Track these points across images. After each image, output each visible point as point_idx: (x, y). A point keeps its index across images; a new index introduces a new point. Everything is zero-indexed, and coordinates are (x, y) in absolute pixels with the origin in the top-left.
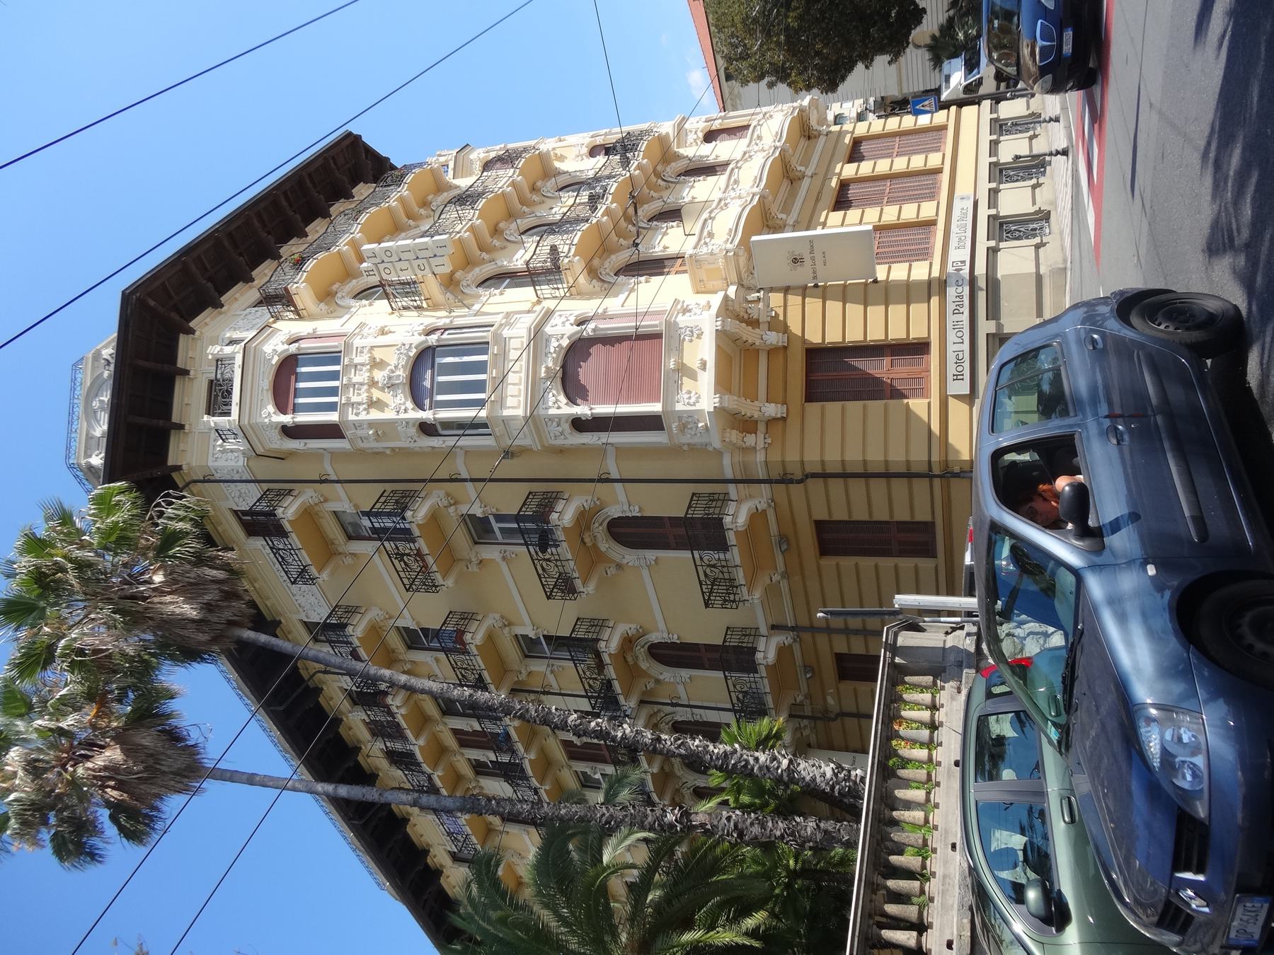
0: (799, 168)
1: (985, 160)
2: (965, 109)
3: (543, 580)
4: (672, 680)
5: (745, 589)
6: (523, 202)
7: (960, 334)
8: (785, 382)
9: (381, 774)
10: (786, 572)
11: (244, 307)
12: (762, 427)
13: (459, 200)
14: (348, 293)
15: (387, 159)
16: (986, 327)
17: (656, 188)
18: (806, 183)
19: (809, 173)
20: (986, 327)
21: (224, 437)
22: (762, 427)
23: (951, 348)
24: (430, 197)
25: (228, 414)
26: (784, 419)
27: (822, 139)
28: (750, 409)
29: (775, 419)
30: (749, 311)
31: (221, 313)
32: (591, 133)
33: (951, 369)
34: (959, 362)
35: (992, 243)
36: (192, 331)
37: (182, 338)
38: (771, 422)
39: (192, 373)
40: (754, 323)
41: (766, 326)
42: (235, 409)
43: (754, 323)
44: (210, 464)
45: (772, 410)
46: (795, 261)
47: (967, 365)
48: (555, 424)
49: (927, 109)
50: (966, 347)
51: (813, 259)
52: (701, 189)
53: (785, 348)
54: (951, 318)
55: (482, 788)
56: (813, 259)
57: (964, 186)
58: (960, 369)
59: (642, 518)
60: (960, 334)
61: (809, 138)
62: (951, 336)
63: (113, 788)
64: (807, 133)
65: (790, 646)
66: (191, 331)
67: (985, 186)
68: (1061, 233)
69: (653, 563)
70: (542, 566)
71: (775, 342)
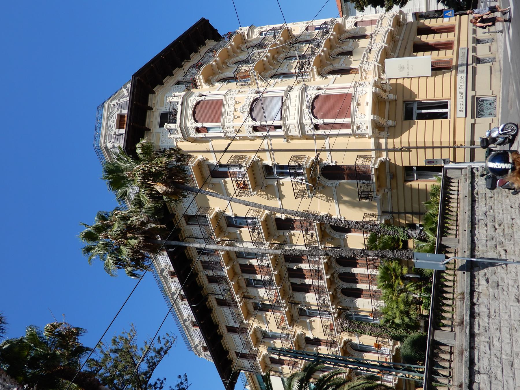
0: (397, 37)
1: (471, 36)
2: (462, 16)
3: (295, 190)
4: (339, 237)
5: (375, 193)
6: (234, 52)
7: (462, 96)
8: (396, 114)
9: (204, 287)
10: (390, 188)
11: (172, 85)
12: (386, 129)
13: (259, 45)
14: (216, 80)
15: (217, 30)
16: (471, 93)
17: (338, 43)
18: (400, 42)
19: (401, 39)
20: (471, 93)
21: (171, 132)
22: (386, 129)
23: (458, 101)
24: (240, 45)
25: (175, 123)
26: (394, 126)
27: (405, 26)
28: (382, 121)
29: (391, 127)
30: (383, 87)
31: (163, 87)
32: (306, 22)
33: (458, 108)
34: (461, 106)
35: (474, 45)
36: (154, 93)
37: (150, 95)
38: (389, 127)
39: (154, 109)
40: (204, 225)
41: (389, 92)
42: (178, 121)
43: (204, 225)
44: (160, 144)
45: (391, 123)
46: (401, 68)
47: (464, 107)
48: (308, 126)
49: (450, 15)
50: (464, 100)
51: (408, 68)
52: (363, 43)
53: (396, 100)
54: (458, 90)
55: (248, 293)
56: (408, 68)
57: (463, 45)
58: (462, 108)
59: (336, 166)
60: (462, 96)
61: (399, 26)
62: (458, 96)
63: (479, 22)
64: (398, 24)
65: (389, 220)
66: (154, 93)
67: (471, 45)
68: (500, 61)
69: (338, 185)
70: (295, 185)
71: (392, 98)
